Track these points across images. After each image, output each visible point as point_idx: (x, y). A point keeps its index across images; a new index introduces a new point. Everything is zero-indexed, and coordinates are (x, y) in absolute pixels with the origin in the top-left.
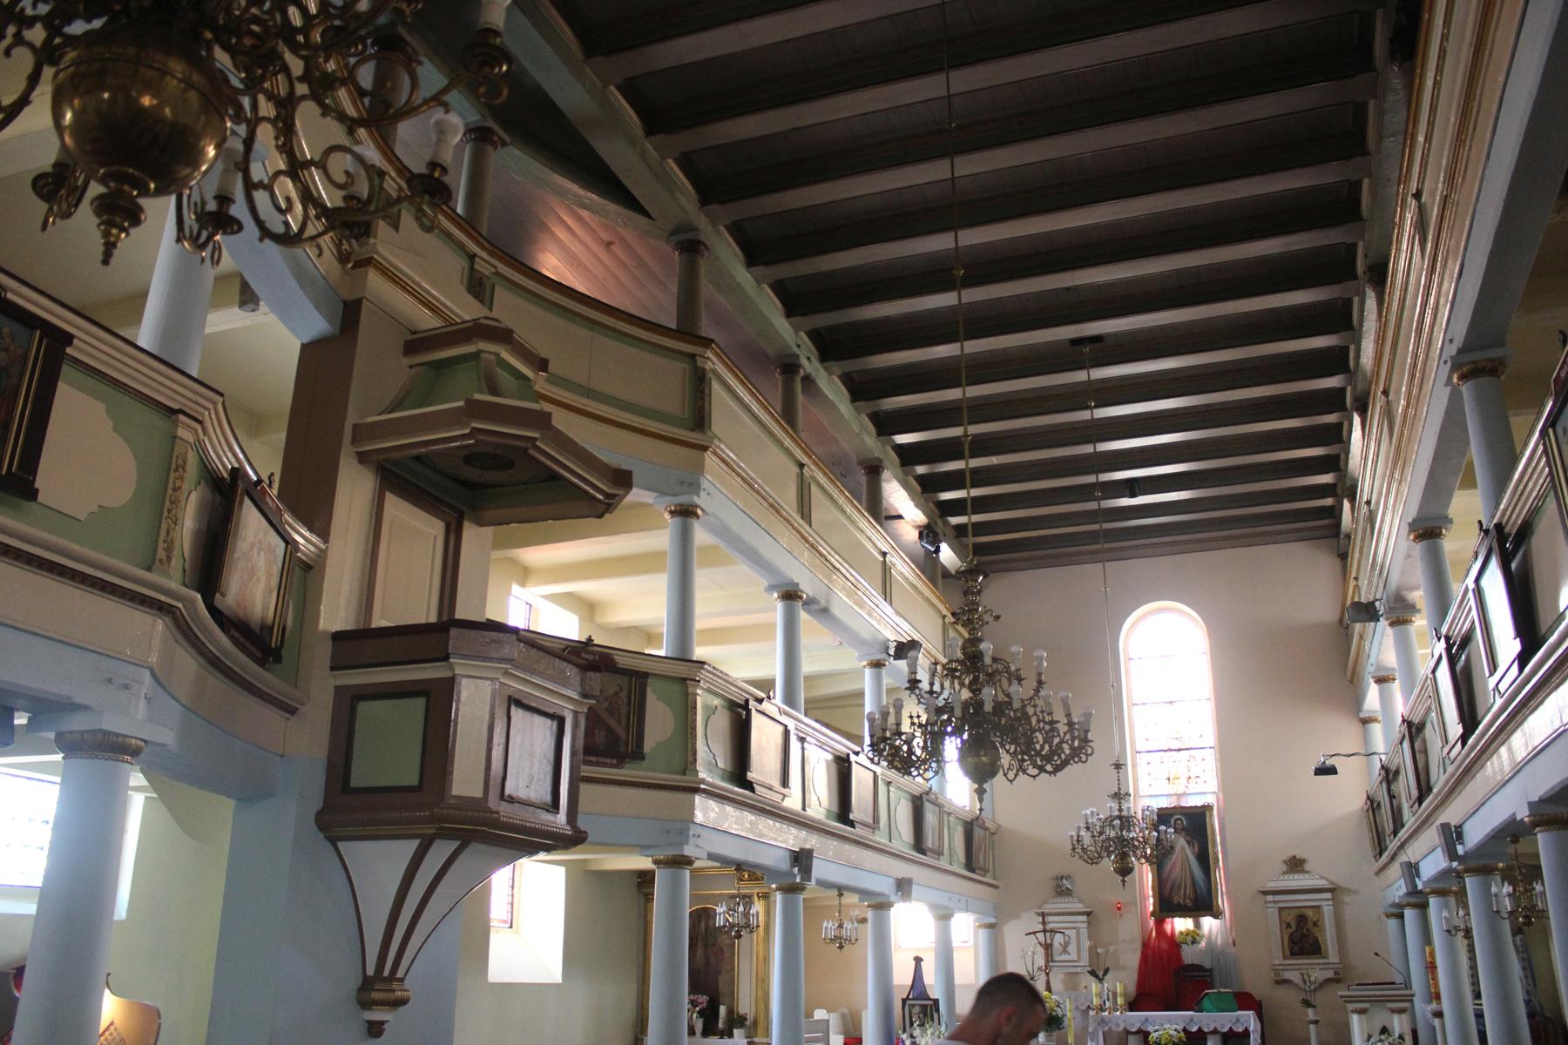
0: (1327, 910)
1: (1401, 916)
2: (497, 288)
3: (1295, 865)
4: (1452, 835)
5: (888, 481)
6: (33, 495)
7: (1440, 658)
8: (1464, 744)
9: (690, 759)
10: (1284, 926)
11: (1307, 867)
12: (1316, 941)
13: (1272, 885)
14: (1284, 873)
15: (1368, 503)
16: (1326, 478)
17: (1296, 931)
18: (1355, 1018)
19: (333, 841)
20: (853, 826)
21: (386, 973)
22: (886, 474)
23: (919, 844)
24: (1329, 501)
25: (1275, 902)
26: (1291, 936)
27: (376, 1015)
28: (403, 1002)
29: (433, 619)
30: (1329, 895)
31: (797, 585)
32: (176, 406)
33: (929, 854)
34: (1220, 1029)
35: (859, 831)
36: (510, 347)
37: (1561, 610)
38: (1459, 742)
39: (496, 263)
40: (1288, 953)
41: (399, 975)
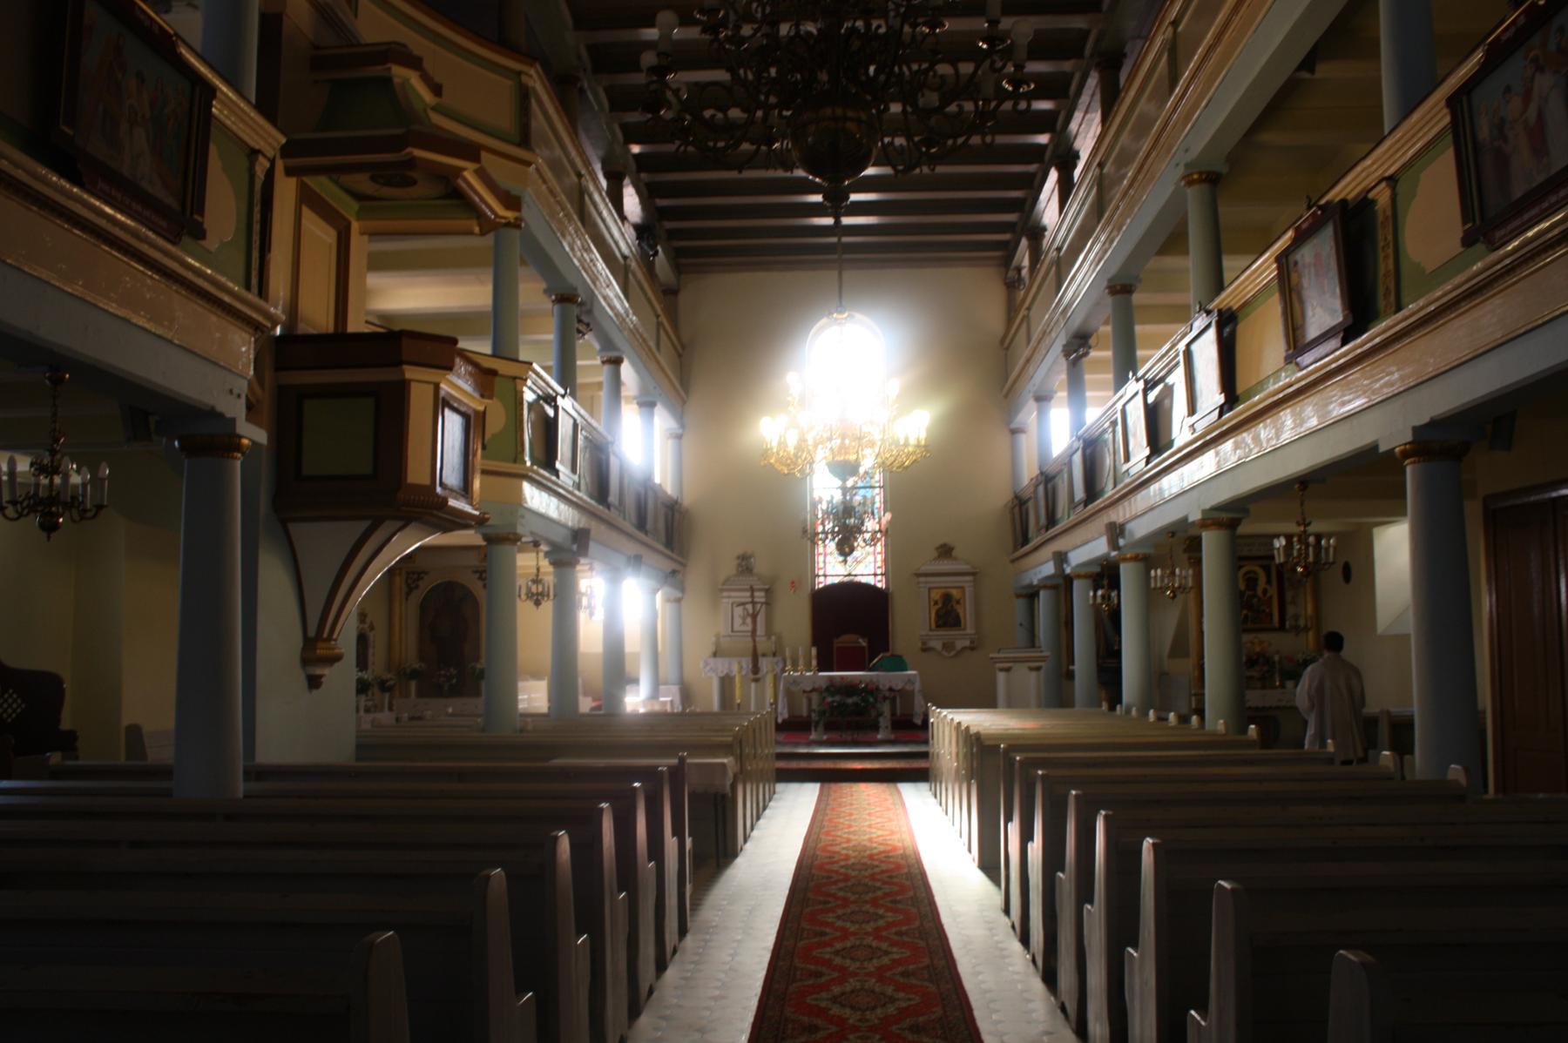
0: (969, 591)
3: (945, 551)
5: (628, 185)
7: (1137, 393)
9: (519, 449)
10: (932, 603)
11: (954, 553)
12: (958, 617)
13: (925, 569)
14: (935, 559)
15: (1059, 249)
16: (1011, 217)
18: (1001, 676)
19: (284, 523)
21: (325, 635)
22: (627, 181)
24: (1007, 237)
25: (926, 583)
29: (331, 330)
31: (576, 289)
32: (257, 147)
36: (418, 73)
37: (1263, 377)
40: (933, 626)
41: (335, 636)
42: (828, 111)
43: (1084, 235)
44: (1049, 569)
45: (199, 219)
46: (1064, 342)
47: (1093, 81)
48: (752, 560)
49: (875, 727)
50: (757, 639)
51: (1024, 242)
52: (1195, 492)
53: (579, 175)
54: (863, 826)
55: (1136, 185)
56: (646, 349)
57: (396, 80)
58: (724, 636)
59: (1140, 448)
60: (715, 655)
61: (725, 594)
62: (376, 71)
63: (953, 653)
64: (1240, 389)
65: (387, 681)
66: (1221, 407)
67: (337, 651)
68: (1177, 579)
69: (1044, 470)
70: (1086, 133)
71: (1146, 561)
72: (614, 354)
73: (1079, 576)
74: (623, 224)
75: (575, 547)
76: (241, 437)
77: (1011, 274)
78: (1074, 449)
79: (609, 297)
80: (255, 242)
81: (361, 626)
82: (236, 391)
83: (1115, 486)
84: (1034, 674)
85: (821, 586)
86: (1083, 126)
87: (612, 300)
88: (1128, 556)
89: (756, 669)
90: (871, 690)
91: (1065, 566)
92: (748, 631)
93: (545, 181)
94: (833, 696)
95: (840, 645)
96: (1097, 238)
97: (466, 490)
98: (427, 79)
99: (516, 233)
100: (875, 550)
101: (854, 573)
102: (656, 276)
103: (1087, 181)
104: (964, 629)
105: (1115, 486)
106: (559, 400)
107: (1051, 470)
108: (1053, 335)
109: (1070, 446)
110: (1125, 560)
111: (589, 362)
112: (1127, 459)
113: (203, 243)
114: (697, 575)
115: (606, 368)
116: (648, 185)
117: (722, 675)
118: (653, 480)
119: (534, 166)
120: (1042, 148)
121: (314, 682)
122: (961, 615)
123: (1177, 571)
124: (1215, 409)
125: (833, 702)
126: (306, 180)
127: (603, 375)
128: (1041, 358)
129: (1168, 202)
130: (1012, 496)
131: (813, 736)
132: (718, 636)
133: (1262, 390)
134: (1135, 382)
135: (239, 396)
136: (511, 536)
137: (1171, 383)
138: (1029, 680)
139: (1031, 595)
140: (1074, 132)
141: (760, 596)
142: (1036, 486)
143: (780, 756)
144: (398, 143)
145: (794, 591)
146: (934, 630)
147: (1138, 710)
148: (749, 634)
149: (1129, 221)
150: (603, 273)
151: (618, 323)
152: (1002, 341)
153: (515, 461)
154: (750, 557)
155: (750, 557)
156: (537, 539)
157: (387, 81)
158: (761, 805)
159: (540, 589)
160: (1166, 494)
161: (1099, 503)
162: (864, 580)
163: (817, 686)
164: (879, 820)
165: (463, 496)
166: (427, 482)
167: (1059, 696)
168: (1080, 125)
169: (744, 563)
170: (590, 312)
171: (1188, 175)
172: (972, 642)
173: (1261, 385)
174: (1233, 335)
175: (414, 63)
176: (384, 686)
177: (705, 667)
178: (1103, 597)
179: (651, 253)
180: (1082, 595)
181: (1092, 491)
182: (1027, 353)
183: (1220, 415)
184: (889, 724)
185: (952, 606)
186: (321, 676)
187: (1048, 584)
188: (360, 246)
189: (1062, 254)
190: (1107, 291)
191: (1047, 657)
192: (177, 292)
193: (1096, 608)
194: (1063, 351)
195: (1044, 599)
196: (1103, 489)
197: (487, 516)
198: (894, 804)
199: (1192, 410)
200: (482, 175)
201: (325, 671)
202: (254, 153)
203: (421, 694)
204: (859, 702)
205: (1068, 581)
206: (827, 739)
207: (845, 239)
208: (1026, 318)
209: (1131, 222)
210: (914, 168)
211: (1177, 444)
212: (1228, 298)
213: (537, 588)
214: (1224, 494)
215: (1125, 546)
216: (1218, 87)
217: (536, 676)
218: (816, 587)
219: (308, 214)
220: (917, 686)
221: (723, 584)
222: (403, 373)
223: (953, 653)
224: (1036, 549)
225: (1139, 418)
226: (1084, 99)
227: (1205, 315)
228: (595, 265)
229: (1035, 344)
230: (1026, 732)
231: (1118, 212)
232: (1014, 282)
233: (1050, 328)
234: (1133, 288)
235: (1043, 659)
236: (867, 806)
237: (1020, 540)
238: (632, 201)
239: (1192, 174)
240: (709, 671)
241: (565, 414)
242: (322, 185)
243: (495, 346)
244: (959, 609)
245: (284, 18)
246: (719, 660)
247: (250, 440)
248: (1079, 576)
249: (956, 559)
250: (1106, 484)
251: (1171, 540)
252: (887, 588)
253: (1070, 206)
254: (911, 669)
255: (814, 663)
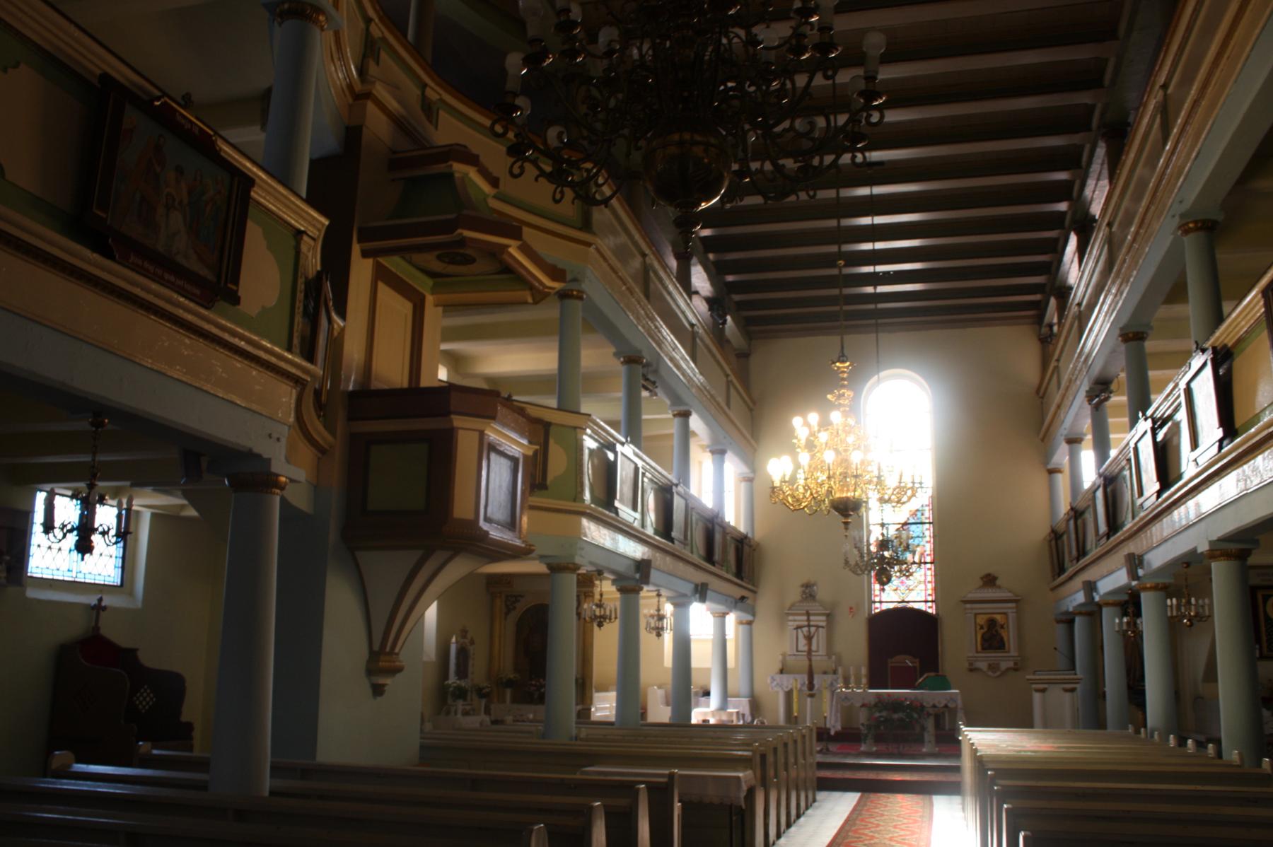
1: (1071, 622)
2: (441, 112)
4: (1135, 562)
5: (695, 265)
6: (235, 300)
7: (1146, 432)
8: (1158, 497)
9: (579, 489)
10: (978, 627)
11: (998, 582)
12: (1002, 640)
13: (971, 596)
14: (981, 587)
15: (1079, 305)
17: (987, 632)
18: (1037, 697)
20: (673, 542)
22: (694, 260)
23: (709, 557)
24: (1038, 297)
25: (972, 609)
26: (983, 635)
27: (381, 681)
28: (399, 670)
29: (405, 384)
30: (1013, 605)
31: (640, 352)
33: (716, 565)
34: (937, 705)
35: (677, 546)
36: (476, 169)
37: (1258, 411)
38: (1156, 494)
39: (441, 92)
40: (979, 648)
42: (676, 137)
43: (1099, 289)
44: (1080, 598)
45: (234, 288)
46: (1087, 389)
47: (1101, 151)
48: (815, 588)
49: (920, 740)
50: (814, 658)
51: (1053, 302)
52: (1203, 524)
53: (644, 255)
54: (885, 838)
55: (1139, 239)
56: (715, 404)
57: (457, 175)
58: (790, 655)
59: (1151, 484)
60: (781, 672)
61: (791, 618)
62: (440, 168)
63: (998, 673)
64: (1238, 423)
65: (484, 688)
66: (1221, 441)
67: (397, 664)
68: (1193, 607)
69: (1074, 506)
70: (1097, 195)
71: (1166, 590)
72: (683, 408)
73: (1107, 604)
74: (690, 299)
75: (638, 576)
76: (278, 475)
77: (1044, 330)
78: (1096, 486)
79: (676, 359)
80: (299, 308)
81: (462, 641)
82: (275, 436)
83: (1133, 518)
84: (1068, 695)
85: (877, 611)
86: (1097, 193)
87: (678, 361)
88: (1148, 585)
89: (811, 686)
90: (917, 708)
91: (1094, 594)
92: (804, 651)
93: (605, 259)
94: (880, 712)
95: (893, 665)
96: (1109, 291)
97: (512, 524)
98: (484, 173)
99: (579, 304)
100: (925, 579)
101: (906, 600)
102: (728, 341)
103: (1099, 240)
104: (1009, 652)
105: (1133, 518)
106: (619, 447)
107: (1081, 505)
108: (1078, 382)
109: (1094, 484)
110: (1145, 589)
111: (657, 414)
112: (1141, 493)
113: (238, 307)
114: (766, 601)
115: (677, 420)
116: (716, 263)
117: (786, 690)
118: (724, 519)
119: (594, 246)
120: (1063, 214)
121: (378, 690)
122: (1005, 639)
123: (1193, 600)
124: (1214, 444)
125: (881, 717)
126: (380, 260)
127: (674, 428)
128: (1069, 403)
129: (1168, 252)
130: (1048, 530)
131: (863, 748)
132: (784, 655)
133: (1259, 422)
134: (1144, 422)
135: (278, 440)
136: (571, 566)
137: (1179, 419)
138: (1063, 701)
139: (1068, 620)
140: (1089, 197)
141: (820, 620)
142: (1068, 520)
143: (821, 766)
144: (449, 227)
145: (853, 616)
146: (980, 652)
147: (1159, 734)
148: (805, 653)
149: (1135, 273)
150: (668, 338)
151: (686, 383)
152: (1038, 391)
153: (575, 500)
154: (813, 585)
155: (813, 585)
156: (600, 568)
157: (450, 176)
158: (793, 812)
159: (602, 613)
160: (1177, 526)
161: (1119, 535)
162: (916, 606)
163: (866, 702)
164: (902, 833)
165: (510, 530)
166: (471, 516)
167: (1094, 718)
168: (1094, 192)
169: (807, 591)
170: (656, 372)
171: (1184, 225)
172: (1016, 664)
173: (1255, 419)
174: (1229, 372)
175: (472, 160)
176: (481, 693)
177: (772, 682)
178: (1128, 623)
179: (720, 322)
180: (1112, 622)
181: (1114, 523)
182: (1057, 399)
183: (1220, 448)
184: (933, 739)
185: (997, 631)
186: (384, 685)
187: (1080, 611)
188: (434, 317)
189: (1082, 308)
190: (1120, 339)
191: (1081, 679)
192: (215, 349)
193: (1124, 634)
194: (1087, 396)
195: (1112, 622)
196: (1123, 522)
197: (532, 548)
198: (922, 817)
199: (1195, 444)
200: (526, 250)
201: (388, 681)
202: (299, 234)
203: (515, 700)
204: (905, 717)
205: (1099, 606)
206: (876, 751)
207: (880, 306)
208: (1057, 368)
209: (1137, 273)
210: (788, 195)
211: (1186, 477)
212: (1224, 334)
213: (600, 612)
214: (1229, 525)
215: (1145, 575)
216: (1205, 139)
217: (604, 689)
218: (873, 612)
219: (383, 289)
220: (959, 702)
221: (790, 609)
222: (451, 421)
223: (998, 673)
224: (1071, 578)
225: (1149, 455)
226: (1095, 167)
227: (1201, 353)
228: (660, 332)
229: (1064, 392)
230: (1038, 755)
231: (1126, 265)
232: (1046, 338)
233: (1075, 376)
234: (1145, 335)
235: (1077, 681)
236: (895, 818)
237: (1057, 571)
238: (700, 279)
239: (1187, 223)
240: (775, 686)
241: (624, 458)
242: (394, 263)
243: (559, 402)
244: (1004, 634)
245: (364, 129)
246: (785, 676)
247: (286, 477)
248: (1107, 604)
249: (999, 587)
250: (1126, 518)
251: (1185, 570)
252: (937, 613)
253: (1086, 264)
254: (955, 689)
255: (864, 680)
